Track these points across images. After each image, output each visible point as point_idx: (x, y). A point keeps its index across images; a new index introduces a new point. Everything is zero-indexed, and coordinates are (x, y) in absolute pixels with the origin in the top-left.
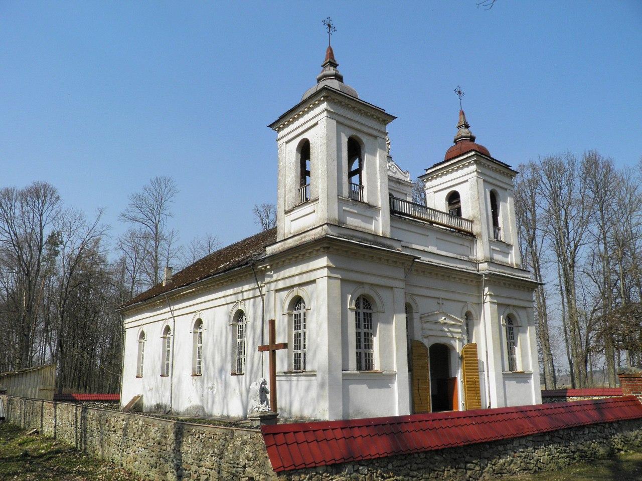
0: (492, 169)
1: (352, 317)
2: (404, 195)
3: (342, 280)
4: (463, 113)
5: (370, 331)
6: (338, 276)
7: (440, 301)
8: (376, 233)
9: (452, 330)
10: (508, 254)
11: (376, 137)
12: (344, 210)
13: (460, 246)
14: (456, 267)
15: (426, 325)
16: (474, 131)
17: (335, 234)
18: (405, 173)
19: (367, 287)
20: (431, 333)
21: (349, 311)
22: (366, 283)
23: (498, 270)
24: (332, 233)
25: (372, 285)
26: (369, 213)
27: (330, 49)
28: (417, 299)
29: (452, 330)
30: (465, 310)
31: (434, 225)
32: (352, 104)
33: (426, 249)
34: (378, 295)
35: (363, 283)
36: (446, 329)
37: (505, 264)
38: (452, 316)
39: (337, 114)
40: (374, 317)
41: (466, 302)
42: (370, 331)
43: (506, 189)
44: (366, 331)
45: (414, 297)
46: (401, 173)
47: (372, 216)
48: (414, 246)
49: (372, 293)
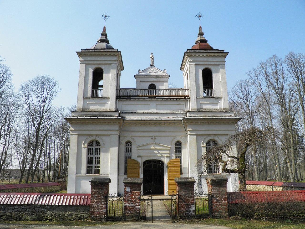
0: (211, 56)
1: (84, 151)
2: (163, 82)
3: (197, 135)
4: (200, 27)
5: (98, 156)
6: (195, 134)
7: (153, 138)
8: (106, 110)
9: (161, 152)
10: (218, 103)
11: (110, 64)
12: (88, 103)
13: (177, 105)
14: (168, 118)
15: (140, 151)
16: (206, 36)
17: (76, 115)
18: (163, 71)
19: (213, 136)
20: (144, 155)
21: (83, 148)
22: (94, 135)
23: (199, 115)
24: (75, 115)
25: (97, 135)
26: (103, 101)
27: (105, 27)
28: (135, 138)
29: (161, 152)
30: (175, 140)
31: (157, 98)
32: (97, 54)
33: (147, 111)
34: (220, 140)
35: (91, 135)
36: (156, 152)
37: (215, 111)
38: (162, 145)
39: (85, 61)
40: (102, 149)
41: (126, 136)
42: (98, 156)
43: (219, 65)
44: (97, 156)
45: (133, 137)
46: (161, 72)
47: (105, 102)
48: (138, 112)
49: (98, 139)
